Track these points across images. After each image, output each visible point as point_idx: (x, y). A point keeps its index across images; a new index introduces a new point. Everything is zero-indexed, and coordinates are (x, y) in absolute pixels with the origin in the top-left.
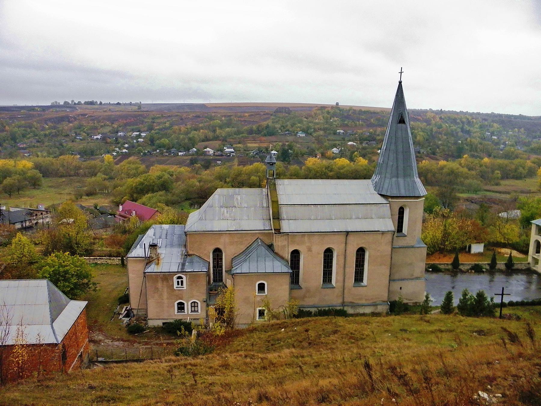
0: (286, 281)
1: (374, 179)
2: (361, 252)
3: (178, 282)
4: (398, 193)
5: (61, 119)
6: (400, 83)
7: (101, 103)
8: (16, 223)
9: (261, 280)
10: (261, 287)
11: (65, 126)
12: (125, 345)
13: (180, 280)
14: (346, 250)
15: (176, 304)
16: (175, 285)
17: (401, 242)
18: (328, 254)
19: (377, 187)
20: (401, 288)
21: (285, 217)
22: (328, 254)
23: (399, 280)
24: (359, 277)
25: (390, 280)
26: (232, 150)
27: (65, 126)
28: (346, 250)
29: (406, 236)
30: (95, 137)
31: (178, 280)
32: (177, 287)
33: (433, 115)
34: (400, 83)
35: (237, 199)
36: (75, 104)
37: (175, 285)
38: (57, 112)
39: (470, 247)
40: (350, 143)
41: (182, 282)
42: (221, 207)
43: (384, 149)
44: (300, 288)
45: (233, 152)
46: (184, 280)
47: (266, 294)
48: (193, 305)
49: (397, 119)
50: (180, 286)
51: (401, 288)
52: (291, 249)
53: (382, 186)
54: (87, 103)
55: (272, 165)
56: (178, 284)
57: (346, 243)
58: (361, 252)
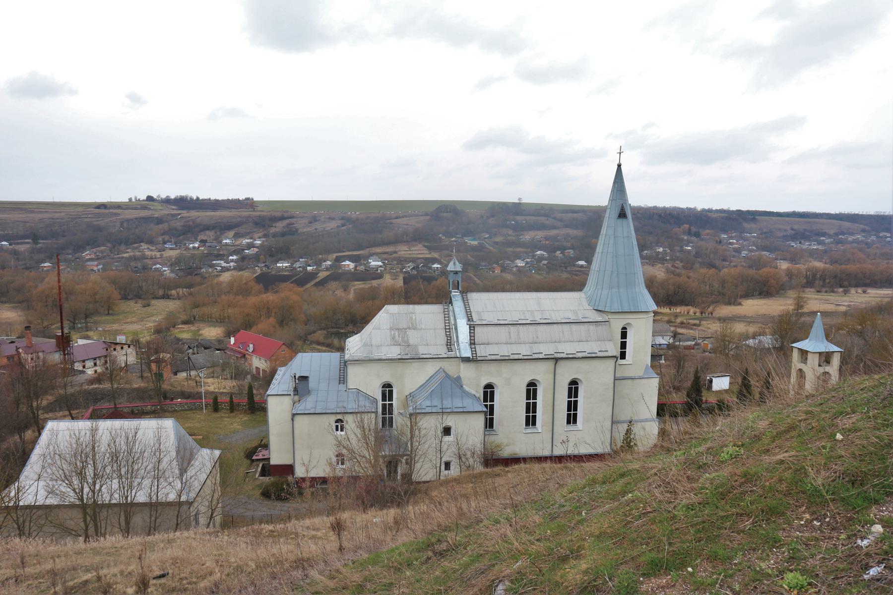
0: (480, 420)
1: (588, 290)
2: (574, 387)
3: (337, 426)
4: (620, 308)
6: (619, 166)
8: (87, 360)
18: (532, 389)
19: (590, 300)
22: (532, 389)
25: (613, 423)
26: (380, 263)
30: (191, 245)
31: (337, 424)
34: (619, 166)
39: (711, 381)
40: (539, 252)
43: (600, 252)
45: (381, 267)
49: (616, 212)
52: (484, 382)
53: (598, 299)
55: (457, 273)
56: (337, 430)
58: (574, 387)
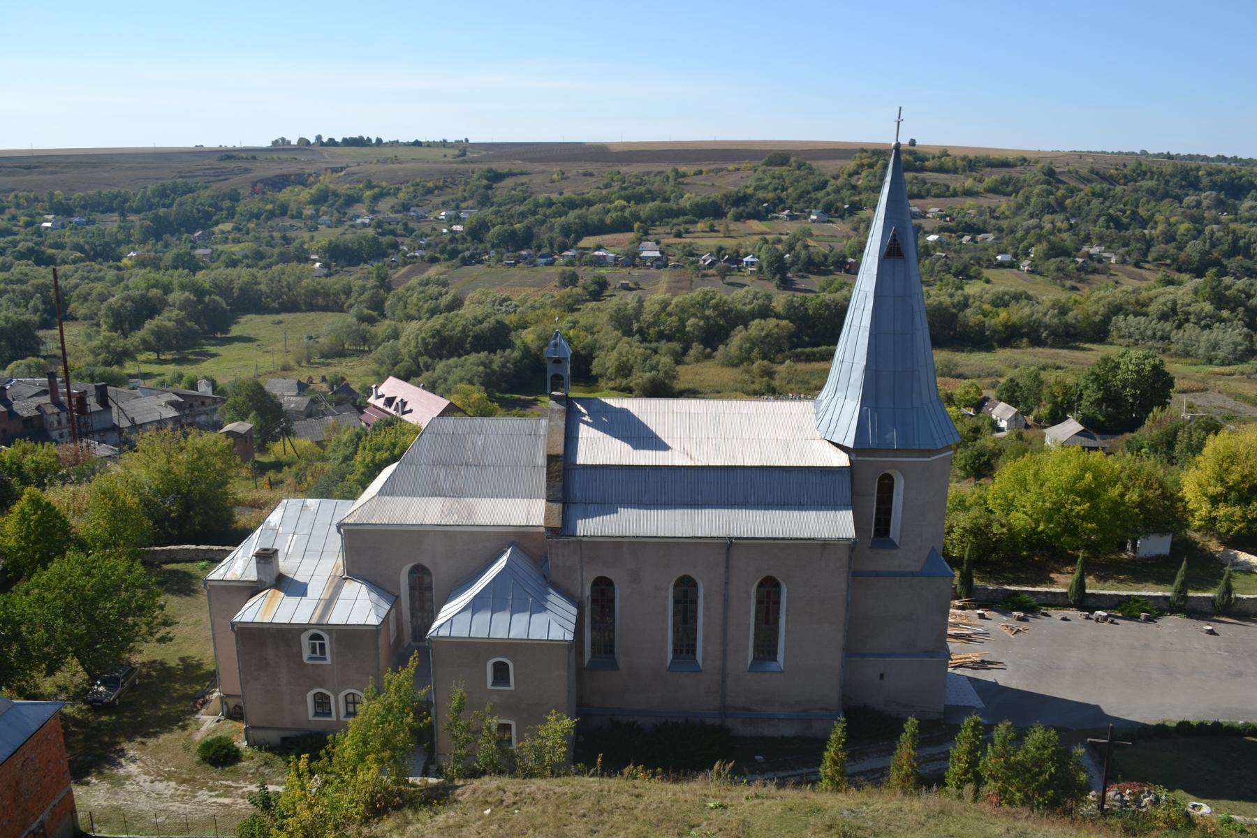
5: (280, 182)
7: (379, 141)
9: (500, 656)
10: (501, 673)
11: (294, 196)
12: (179, 792)
13: (317, 642)
14: (726, 583)
15: (310, 696)
16: (306, 653)
17: (886, 561)
20: (882, 676)
21: (578, 495)
23: (875, 655)
24: (766, 648)
27: (294, 196)
28: (726, 583)
29: (701, 671)
32: (310, 659)
33: (686, 375)
35: (474, 444)
36: (322, 144)
37: (306, 653)
38: (280, 161)
41: (322, 646)
42: (435, 464)
44: (615, 666)
46: (327, 642)
47: (512, 687)
48: (350, 698)
50: (318, 654)
51: (882, 676)
54: (350, 142)
56: (314, 651)
57: (727, 567)
